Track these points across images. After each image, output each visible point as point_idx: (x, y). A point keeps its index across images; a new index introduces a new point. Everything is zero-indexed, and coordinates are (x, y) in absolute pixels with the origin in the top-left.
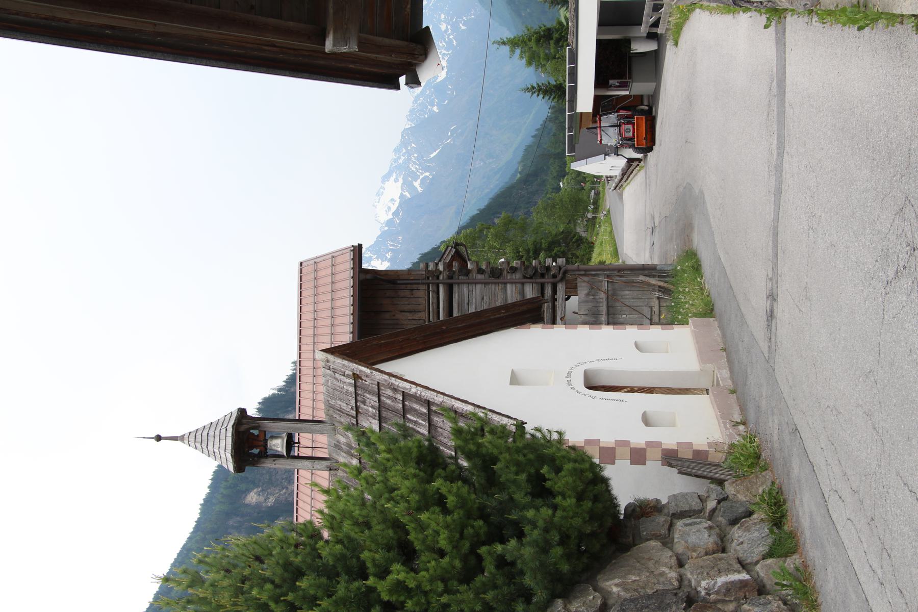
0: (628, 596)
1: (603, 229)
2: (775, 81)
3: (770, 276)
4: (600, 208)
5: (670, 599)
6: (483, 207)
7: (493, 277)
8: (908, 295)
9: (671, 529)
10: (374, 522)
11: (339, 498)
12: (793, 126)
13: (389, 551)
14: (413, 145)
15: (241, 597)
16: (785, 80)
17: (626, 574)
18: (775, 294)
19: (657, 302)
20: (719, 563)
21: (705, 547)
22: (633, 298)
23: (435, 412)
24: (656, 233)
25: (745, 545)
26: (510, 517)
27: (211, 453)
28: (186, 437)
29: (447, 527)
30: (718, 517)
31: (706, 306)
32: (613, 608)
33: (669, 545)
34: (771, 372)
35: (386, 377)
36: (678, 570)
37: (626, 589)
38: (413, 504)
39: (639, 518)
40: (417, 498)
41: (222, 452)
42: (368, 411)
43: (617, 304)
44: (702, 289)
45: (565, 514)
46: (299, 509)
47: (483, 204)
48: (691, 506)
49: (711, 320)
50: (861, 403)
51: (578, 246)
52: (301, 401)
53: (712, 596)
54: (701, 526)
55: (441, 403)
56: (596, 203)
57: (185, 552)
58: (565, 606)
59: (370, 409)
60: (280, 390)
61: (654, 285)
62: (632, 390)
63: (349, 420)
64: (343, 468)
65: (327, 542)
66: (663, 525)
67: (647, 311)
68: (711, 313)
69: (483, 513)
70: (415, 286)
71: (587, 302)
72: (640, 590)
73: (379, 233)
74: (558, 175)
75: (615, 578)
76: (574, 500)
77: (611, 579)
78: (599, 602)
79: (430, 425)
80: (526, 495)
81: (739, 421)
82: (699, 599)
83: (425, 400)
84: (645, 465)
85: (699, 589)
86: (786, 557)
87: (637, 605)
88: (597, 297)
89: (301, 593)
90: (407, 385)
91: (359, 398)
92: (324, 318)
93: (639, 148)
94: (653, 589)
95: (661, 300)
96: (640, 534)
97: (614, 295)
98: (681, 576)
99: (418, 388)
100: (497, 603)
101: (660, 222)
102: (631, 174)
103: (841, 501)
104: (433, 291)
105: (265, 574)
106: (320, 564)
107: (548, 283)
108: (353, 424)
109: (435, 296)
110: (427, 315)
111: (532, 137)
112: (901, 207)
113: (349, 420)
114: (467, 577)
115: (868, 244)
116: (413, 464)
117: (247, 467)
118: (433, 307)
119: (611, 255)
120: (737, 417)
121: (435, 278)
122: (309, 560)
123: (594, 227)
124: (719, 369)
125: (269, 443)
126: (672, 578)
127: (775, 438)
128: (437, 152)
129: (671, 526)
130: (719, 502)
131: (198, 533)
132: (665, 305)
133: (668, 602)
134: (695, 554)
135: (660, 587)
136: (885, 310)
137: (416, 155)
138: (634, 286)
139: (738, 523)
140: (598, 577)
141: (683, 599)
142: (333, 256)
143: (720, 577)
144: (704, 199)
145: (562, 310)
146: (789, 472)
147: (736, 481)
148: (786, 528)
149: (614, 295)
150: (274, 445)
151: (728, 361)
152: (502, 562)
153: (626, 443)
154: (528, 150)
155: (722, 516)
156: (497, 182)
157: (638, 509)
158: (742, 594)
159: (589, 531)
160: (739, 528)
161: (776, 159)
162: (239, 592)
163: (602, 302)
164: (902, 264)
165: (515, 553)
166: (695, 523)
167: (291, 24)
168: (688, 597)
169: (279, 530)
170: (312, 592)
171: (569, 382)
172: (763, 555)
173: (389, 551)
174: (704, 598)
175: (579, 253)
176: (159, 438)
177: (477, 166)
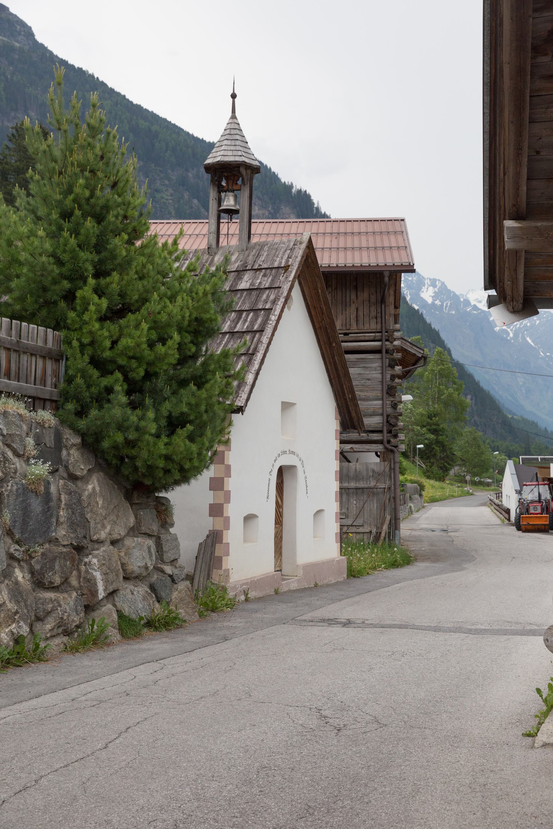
0: (84, 497)
1: (456, 489)
2: (537, 628)
3: (366, 622)
4: (475, 487)
5: (81, 532)
6: (481, 385)
7: (388, 388)
8: (302, 725)
9: (146, 536)
10: (145, 282)
11: (170, 253)
12: (489, 641)
13: (119, 295)
14: (538, 322)
15: (79, 169)
16: (534, 635)
17: (103, 496)
18: (349, 625)
19: (368, 531)
20: (114, 574)
21: (129, 563)
22: (370, 510)
23: (254, 337)
24: (442, 533)
25: (131, 596)
26: (147, 398)
27: (221, 143)
28: (235, 121)
29: (138, 345)
30: (157, 575)
31: (358, 571)
32: (74, 486)
33: (131, 533)
34: (283, 621)
35: (285, 294)
36: (108, 540)
37: (90, 496)
38: (159, 317)
39: (156, 509)
40: (163, 320)
41: (222, 153)
42: (257, 279)
43: (365, 496)
44: (374, 568)
45: (152, 444)
46: (190, 224)
47: (484, 385)
48: (167, 552)
49: (345, 576)
50: (227, 688)
51: (441, 468)
52: (282, 224)
53: (84, 567)
54: (148, 560)
55: (261, 342)
56: (480, 483)
57: (176, 130)
58: (74, 445)
59: (258, 281)
60: (317, 209)
61: (382, 528)
62: (279, 506)
63: (250, 263)
64: (210, 259)
65: (451, 301)
66: (149, 529)
67: (359, 522)
68: (352, 576)
69: (148, 376)
70: (379, 320)
71: (367, 470)
72: (89, 507)
73: (458, 293)
74: (510, 451)
75: (100, 487)
76: (164, 452)
77: (99, 484)
78: (78, 473)
79: (244, 332)
80: (169, 411)
81: (249, 596)
82: (81, 557)
83: (264, 328)
84: (210, 516)
85: (90, 556)
86: (119, 630)
87: (75, 504)
88: (371, 479)
89: (82, 221)
90: (277, 312)
91: (268, 271)
92: (353, 241)
93: (519, 519)
94: (91, 519)
95: (369, 534)
96: (141, 509)
97: (373, 493)
98: (102, 542)
99: (275, 322)
100: (75, 387)
101: (450, 536)
102: (500, 512)
103: (152, 671)
104: (375, 336)
105: (97, 190)
106: (108, 237)
107: (383, 436)
108: (246, 266)
109: (372, 338)
110: (354, 331)
111: (546, 428)
112: (379, 721)
113: (250, 263)
114: (95, 362)
115: (359, 696)
116: (194, 315)
117: (210, 175)
118: (361, 336)
119: (432, 496)
120: (252, 594)
121: (387, 338)
122: (111, 227)
123: (459, 482)
124: (298, 581)
125: (231, 194)
126: (100, 534)
127: (225, 624)
128: (532, 344)
129: (150, 536)
130: (171, 576)
131: (193, 142)
132: (365, 537)
133: (78, 531)
134: (122, 554)
135: (92, 524)
136: (297, 708)
137: (528, 324)
138: (381, 512)
139: (152, 591)
140: (101, 474)
141: (81, 543)
142: (406, 248)
143: (101, 575)
144: (456, 571)
145: (359, 449)
146: (193, 634)
147: (190, 591)
148: (145, 630)
149: (373, 493)
150: (228, 199)
151: (305, 589)
152: (109, 390)
153: (227, 499)
154: (534, 424)
155: (158, 578)
156: (504, 397)
157: (164, 508)
158: (85, 591)
159: (137, 464)
160: (147, 592)
161: (466, 628)
162: (83, 168)
163: (367, 483)
164: (331, 721)
165: (116, 402)
166: (151, 555)
167: (525, 188)
168: (83, 547)
169: (141, 202)
170: (82, 231)
171: (284, 452)
172: (121, 611)
173: (119, 295)
174: (82, 560)
175: (435, 468)
176: (234, 96)
177: (518, 379)
